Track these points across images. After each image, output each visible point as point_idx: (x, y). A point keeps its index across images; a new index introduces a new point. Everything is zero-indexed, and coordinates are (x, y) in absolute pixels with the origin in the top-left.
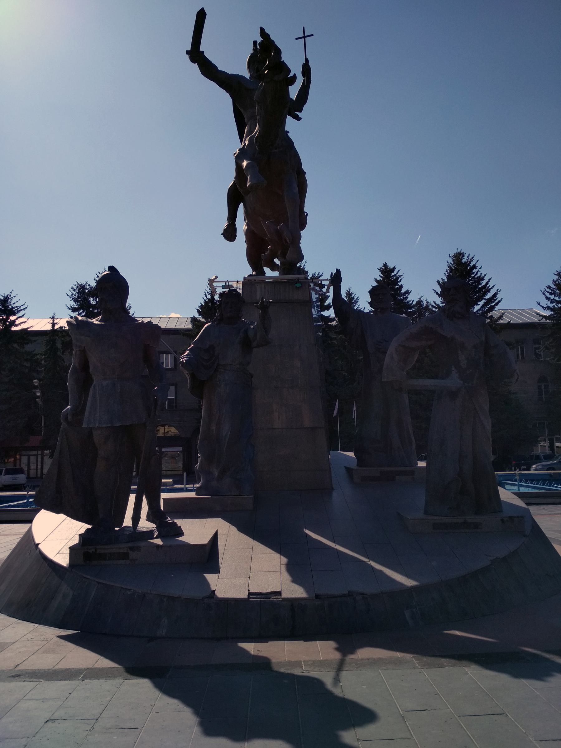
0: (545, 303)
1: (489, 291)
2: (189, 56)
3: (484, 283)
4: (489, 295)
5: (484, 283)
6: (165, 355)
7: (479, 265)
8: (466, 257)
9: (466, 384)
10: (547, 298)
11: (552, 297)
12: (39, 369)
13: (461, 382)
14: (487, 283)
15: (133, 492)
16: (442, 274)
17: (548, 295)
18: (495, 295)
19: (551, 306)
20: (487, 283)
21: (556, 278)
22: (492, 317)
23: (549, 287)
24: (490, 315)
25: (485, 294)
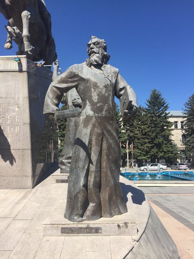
0: (185, 108)
1: (165, 104)
2: (119, 181)
3: (163, 101)
4: (165, 105)
5: (163, 101)
6: (69, 170)
7: (161, 94)
8: (157, 91)
9: (96, 115)
10: (186, 107)
11: (188, 106)
12: (104, 113)
13: (93, 113)
14: (164, 101)
15: (97, 106)
16: (148, 98)
17: (186, 106)
18: (167, 105)
19: (188, 109)
20: (164, 101)
21: (189, 99)
22: (166, 113)
23: (186, 103)
24: (165, 112)
25: (164, 105)
